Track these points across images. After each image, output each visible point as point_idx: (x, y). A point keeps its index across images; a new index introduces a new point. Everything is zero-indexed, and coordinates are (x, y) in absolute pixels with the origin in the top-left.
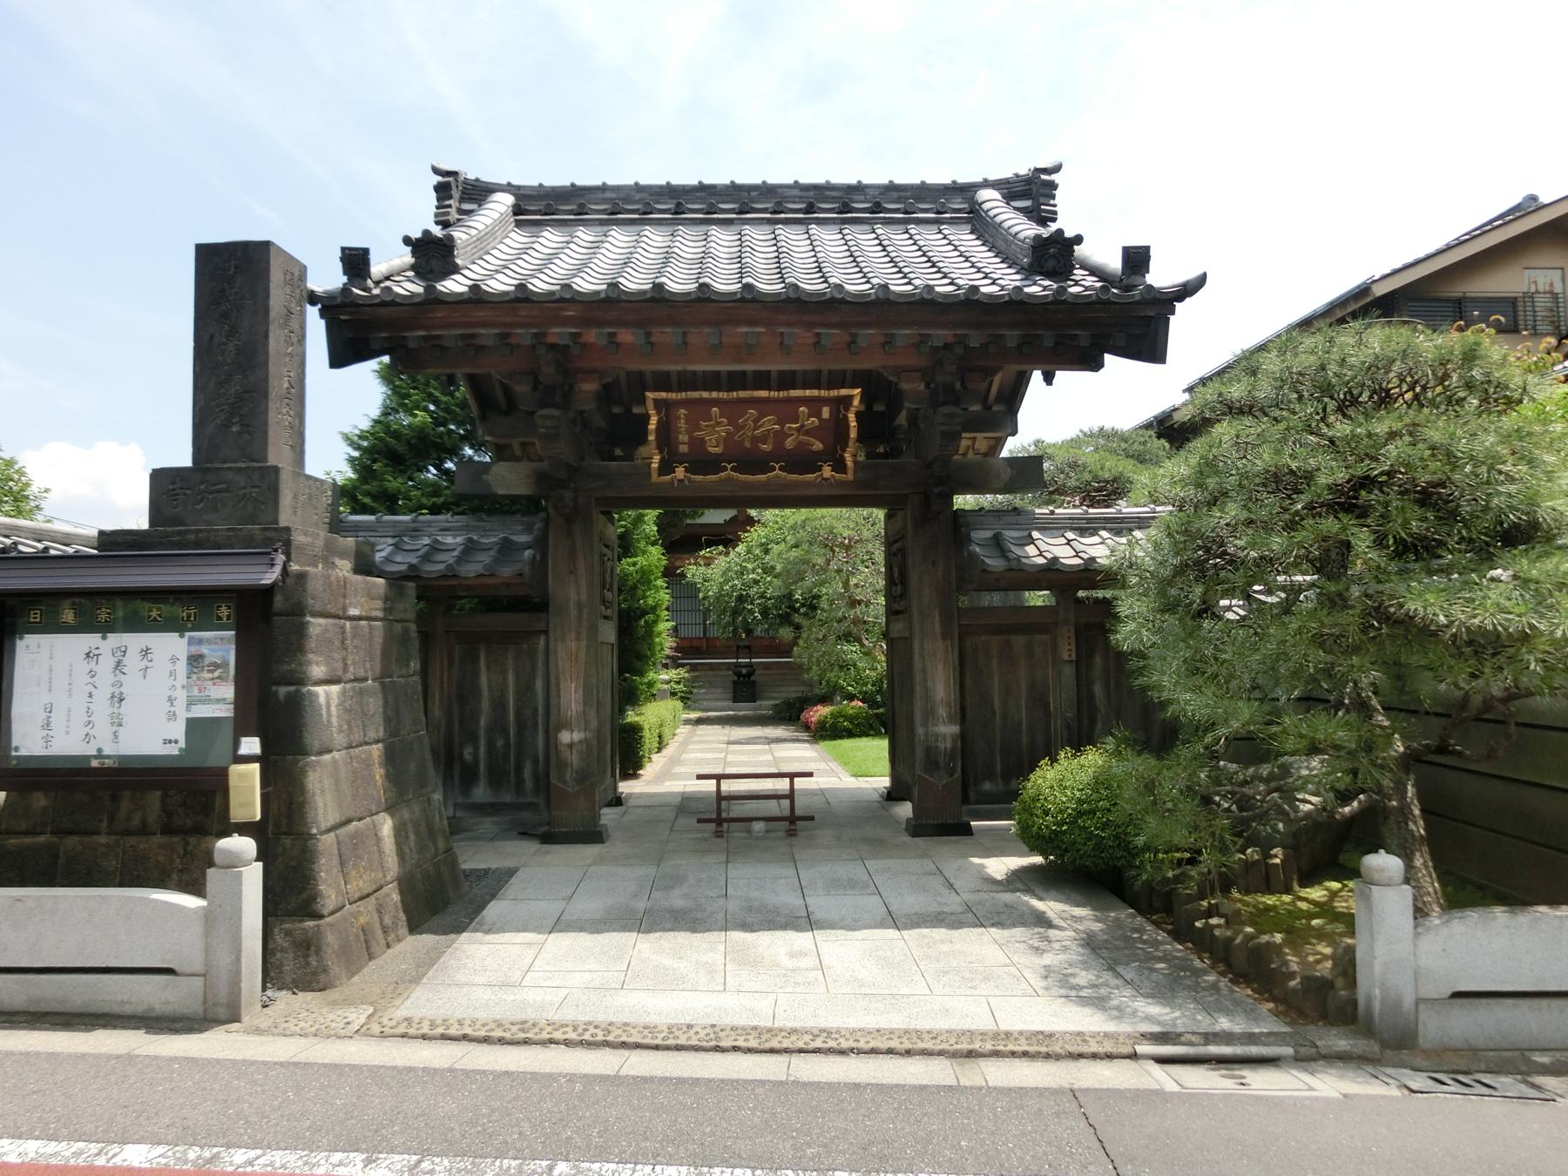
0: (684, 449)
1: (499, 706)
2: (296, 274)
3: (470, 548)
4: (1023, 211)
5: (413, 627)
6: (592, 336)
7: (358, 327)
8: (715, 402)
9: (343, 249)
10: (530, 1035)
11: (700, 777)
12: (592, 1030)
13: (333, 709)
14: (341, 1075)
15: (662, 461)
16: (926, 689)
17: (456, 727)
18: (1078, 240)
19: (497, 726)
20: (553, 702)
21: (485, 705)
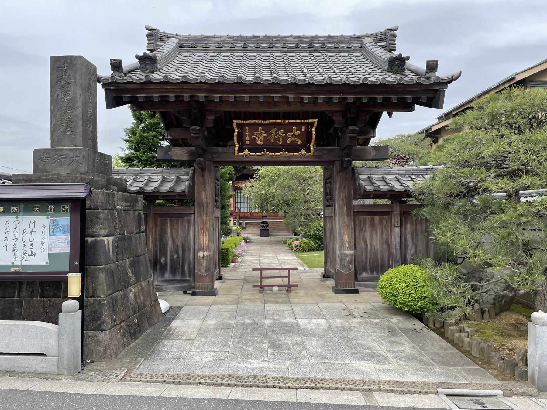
0: (248, 143)
1: (175, 242)
2: (92, 71)
3: (164, 180)
4: (383, 47)
5: (142, 212)
6: (216, 97)
7: (117, 95)
9: (111, 60)
10: (191, 381)
11: (254, 270)
12: (216, 379)
13: (111, 247)
14: (115, 400)
15: (239, 147)
18: (408, 58)
20: (197, 240)
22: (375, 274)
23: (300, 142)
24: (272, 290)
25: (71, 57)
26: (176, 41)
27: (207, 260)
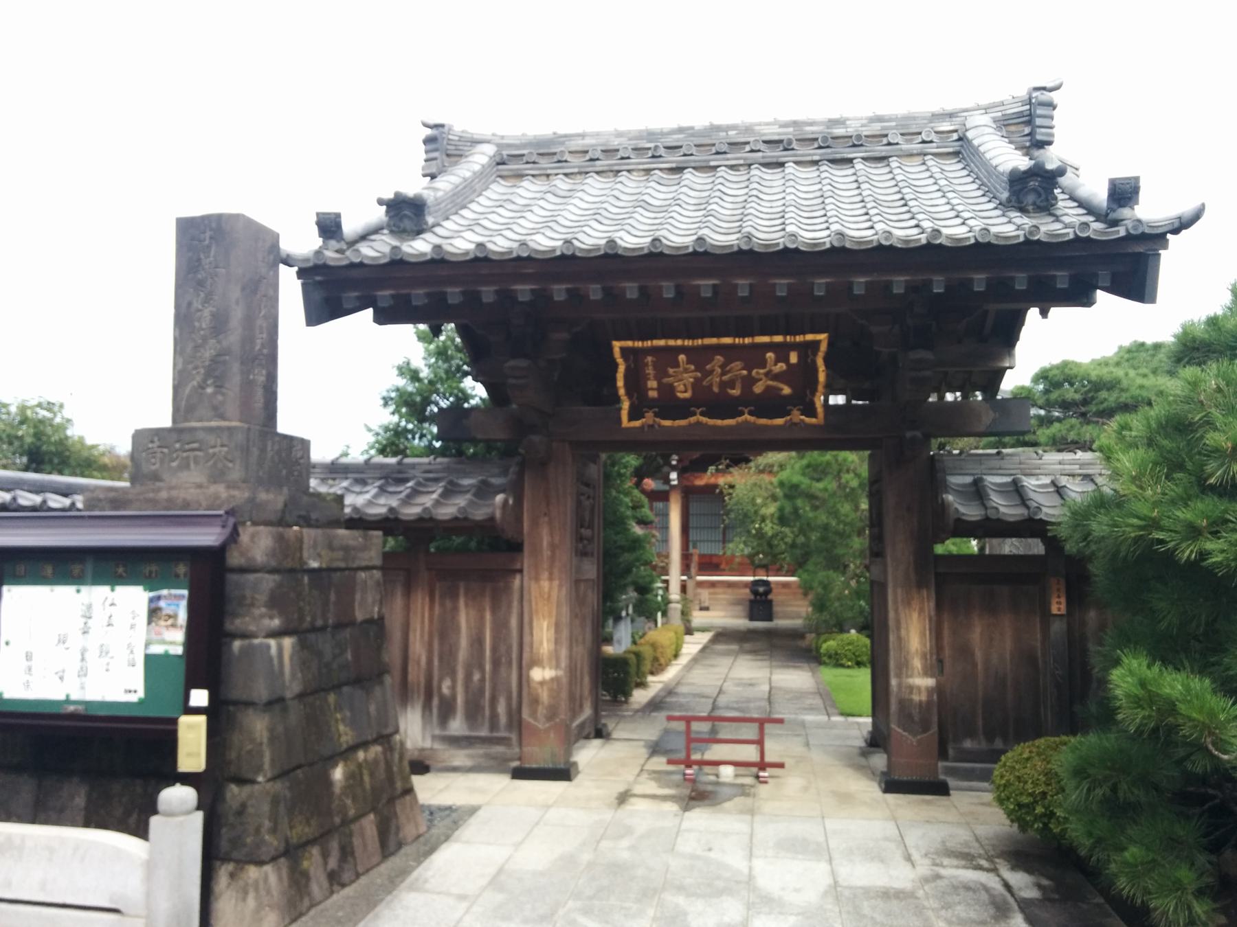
0: (653, 394)
8: (682, 350)
16: (899, 638)
17: (436, 662)
19: (476, 661)
20: (526, 639)
21: (464, 642)
22: (998, 744)
23: (787, 390)
24: (717, 776)
25: (219, 218)
26: (490, 149)
27: (551, 690)
